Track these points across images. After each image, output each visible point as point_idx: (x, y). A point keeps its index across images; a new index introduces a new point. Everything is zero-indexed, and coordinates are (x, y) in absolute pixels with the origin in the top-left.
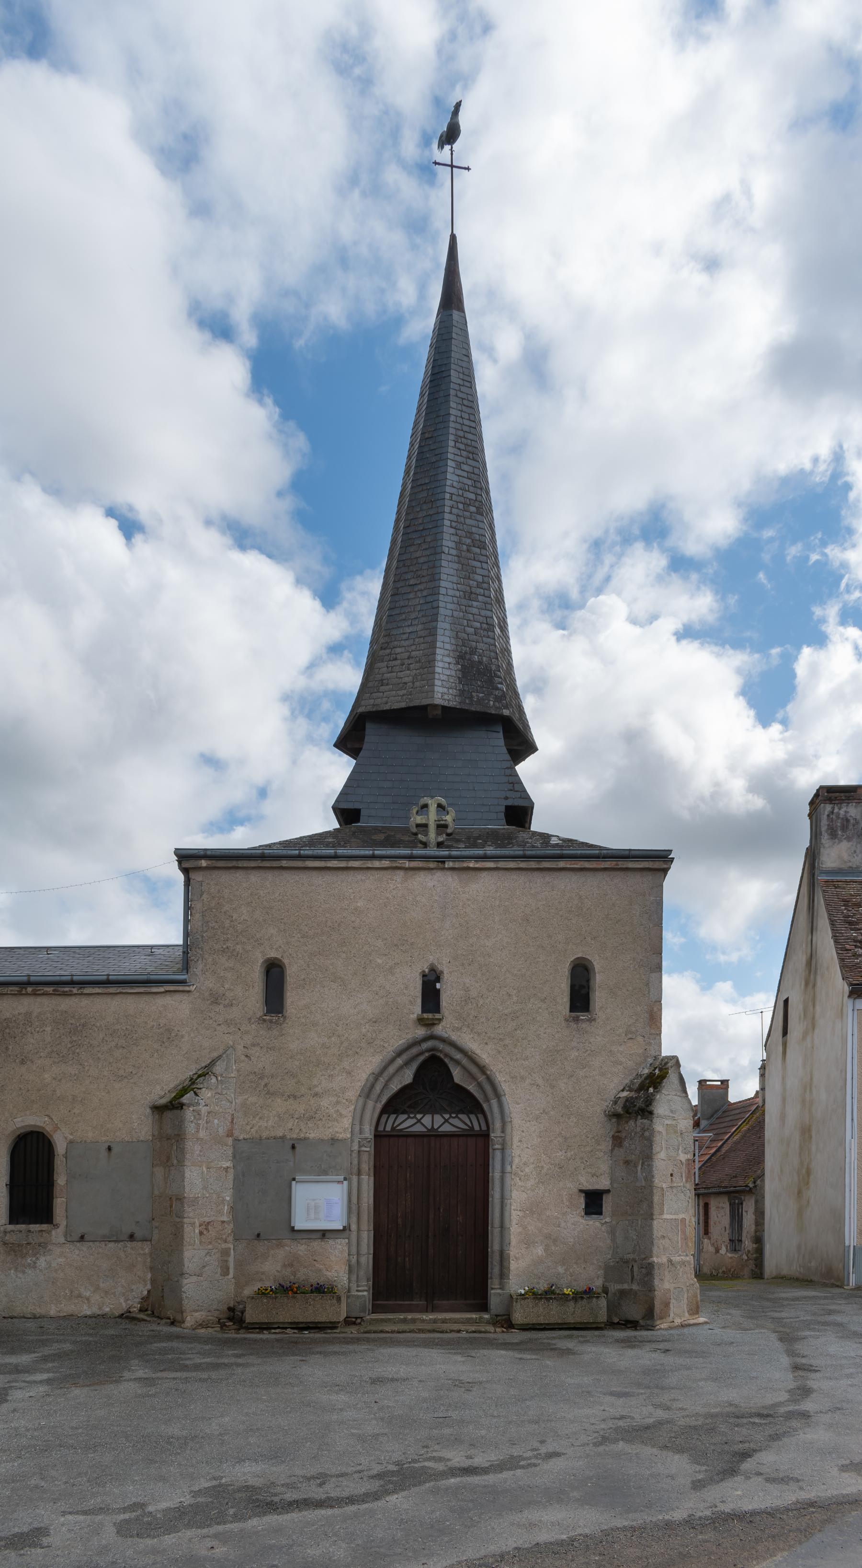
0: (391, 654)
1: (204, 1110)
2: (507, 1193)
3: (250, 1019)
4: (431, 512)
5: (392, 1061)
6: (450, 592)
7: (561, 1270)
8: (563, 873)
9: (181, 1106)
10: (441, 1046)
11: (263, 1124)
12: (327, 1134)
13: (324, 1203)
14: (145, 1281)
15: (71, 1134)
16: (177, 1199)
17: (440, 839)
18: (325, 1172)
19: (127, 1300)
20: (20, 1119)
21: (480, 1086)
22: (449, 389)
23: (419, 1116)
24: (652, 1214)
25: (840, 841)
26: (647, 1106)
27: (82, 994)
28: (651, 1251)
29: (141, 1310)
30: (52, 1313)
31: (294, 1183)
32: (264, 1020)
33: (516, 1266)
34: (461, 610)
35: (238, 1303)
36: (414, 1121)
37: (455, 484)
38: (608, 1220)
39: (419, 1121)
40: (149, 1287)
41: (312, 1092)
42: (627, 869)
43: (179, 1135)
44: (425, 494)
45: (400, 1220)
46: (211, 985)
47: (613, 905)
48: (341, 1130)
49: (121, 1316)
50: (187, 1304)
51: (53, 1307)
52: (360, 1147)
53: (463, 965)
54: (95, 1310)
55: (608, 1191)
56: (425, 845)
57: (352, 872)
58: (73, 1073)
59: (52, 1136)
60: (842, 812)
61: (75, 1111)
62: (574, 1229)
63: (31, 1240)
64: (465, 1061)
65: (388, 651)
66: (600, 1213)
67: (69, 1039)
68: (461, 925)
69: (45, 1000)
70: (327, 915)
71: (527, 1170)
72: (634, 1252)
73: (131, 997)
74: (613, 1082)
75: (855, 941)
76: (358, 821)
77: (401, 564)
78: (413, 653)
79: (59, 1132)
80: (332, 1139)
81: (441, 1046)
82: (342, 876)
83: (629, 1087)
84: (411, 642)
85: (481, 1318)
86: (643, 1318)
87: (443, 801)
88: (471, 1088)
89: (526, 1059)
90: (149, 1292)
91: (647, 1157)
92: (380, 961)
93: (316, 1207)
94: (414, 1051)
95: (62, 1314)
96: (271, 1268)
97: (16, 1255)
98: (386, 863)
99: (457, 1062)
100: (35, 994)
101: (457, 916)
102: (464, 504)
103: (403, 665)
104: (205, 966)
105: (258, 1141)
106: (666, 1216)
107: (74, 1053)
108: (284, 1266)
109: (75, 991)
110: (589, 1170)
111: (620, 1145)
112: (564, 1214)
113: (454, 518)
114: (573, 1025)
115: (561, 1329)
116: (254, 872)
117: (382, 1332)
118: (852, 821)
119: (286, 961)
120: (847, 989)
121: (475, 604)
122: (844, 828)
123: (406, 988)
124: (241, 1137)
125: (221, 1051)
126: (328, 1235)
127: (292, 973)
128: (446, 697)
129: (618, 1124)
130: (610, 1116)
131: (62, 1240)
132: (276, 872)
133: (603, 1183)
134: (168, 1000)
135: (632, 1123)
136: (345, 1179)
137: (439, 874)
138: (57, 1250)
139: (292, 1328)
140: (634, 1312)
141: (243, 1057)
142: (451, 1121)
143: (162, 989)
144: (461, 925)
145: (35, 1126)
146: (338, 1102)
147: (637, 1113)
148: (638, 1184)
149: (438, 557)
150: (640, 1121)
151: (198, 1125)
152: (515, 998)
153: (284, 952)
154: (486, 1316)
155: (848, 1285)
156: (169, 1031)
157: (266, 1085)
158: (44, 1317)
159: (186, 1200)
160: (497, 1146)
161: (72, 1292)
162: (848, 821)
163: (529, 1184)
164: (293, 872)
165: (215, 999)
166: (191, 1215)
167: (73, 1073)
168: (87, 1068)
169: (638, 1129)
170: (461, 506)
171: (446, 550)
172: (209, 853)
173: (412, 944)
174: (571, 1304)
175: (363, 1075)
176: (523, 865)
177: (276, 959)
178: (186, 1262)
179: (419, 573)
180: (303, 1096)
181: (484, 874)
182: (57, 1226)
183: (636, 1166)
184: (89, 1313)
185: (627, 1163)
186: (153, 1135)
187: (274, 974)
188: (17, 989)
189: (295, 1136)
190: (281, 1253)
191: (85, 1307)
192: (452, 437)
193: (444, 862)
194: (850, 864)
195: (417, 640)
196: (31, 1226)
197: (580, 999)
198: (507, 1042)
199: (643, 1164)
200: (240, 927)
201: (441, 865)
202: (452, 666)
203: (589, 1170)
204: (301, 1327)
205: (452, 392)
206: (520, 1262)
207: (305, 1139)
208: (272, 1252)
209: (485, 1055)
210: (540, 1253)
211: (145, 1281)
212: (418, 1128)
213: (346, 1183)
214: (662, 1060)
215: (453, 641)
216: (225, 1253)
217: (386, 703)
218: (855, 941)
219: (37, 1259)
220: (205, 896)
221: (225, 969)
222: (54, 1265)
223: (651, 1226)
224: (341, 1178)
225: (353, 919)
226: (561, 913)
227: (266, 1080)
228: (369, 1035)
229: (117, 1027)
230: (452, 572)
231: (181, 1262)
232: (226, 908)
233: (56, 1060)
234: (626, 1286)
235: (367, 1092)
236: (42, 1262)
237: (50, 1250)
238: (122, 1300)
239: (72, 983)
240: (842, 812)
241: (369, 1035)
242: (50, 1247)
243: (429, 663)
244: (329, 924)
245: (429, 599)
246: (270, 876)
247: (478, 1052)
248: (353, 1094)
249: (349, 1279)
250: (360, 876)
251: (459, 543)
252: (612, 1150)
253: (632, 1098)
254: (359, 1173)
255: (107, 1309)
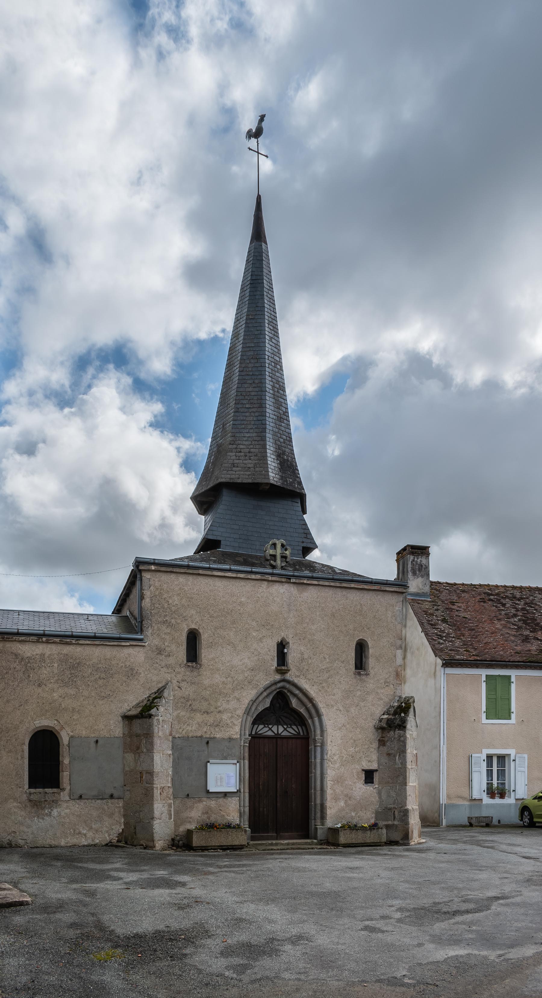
0: (236, 448)
1: (161, 719)
2: (325, 771)
3: (180, 665)
4: (257, 365)
5: (262, 693)
6: (271, 416)
7: (353, 814)
8: (352, 590)
9: (150, 716)
10: (288, 686)
11: (189, 728)
12: (226, 735)
13: (226, 776)
14: (120, 823)
15: (72, 732)
16: (146, 773)
17: (283, 565)
18: (225, 758)
19: (109, 835)
20: (38, 722)
21: (308, 710)
22: (263, 291)
23: (270, 726)
24: (406, 783)
25: (418, 577)
26: (403, 723)
27: (78, 644)
28: (406, 803)
29: (118, 841)
30: (63, 843)
31: (208, 764)
32: (188, 666)
33: (330, 812)
34: (276, 428)
35: (176, 836)
36: (267, 729)
37: (270, 350)
38: (377, 786)
39: (270, 729)
40: (123, 827)
41: (218, 710)
42: (385, 591)
43: (147, 734)
44: (252, 353)
45: (261, 787)
46: (157, 643)
47: (378, 610)
48: (234, 733)
49: (107, 845)
50: (156, 837)
51: (63, 840)
52: (244, 743)
53: (300, 639)
54: (90, 842)
55: (376, 770)
56: (274, 567)
57: (238, 580)
58: (72, 693)
59: (59, 733)
60: (419, 561)
61: (74, 717)
62: (360, 791)
63: (47, 799)
64: (300, 695)
65: (235, 446)
66: (373, 783)
67: (69, 672)
68: (299, 616)
69: (53, 647)
70: (225, 605)
71: (335, 758)
72: (394, 804)
73: (108, 648)
74: (376, 709)
75: (437, 635)
76: (219, 547)
77: (239, 394)
78: (252, 450)
79: (64, 730)
80: (230, 738)
81: (288, 686)
82: (233, 582)
83: (387, 712)
84: (250, 443)
85: (312, 842)
86: (402, 840)
87: (284, 542)
88: (302, 710)
89: (334, 695)
90: (123, 830)
91: (403, 751)
92: (254, 634)
93: (221, 779)
94: (273, 688)
95: (68, 845)
96: (196, 814)
97: (38, 808)
98: (258, 577)
99: (295, 695)
100: (47, 642)
101: (296, 610)
102: (274, 363)
103: (246, 456)
104: (153, 631)
105: (186, 739)
106: (411, 784)
107: (73, 681)
108: (203, 813)
109: (74, 642)
110: (367, 759)
111: (384, 745)
112: (355, 783)
113: (270, 371)
114: (358, 677)
115: (362, 846)
116: (181, 575)
117: (272, 850)
118: (424, 566)
119: (201, 631)
120: (439, 662)
121: (283, 424)
122: (420, 570)
123: (269, 651)
124: (177, 736)
125: (163, 684)
126: (228, 795)
127: (205, 637)
128: (275, 479)
129: (382, 733)
130: (378, 728)
131: (67, 798)
132: (195, 577)
133: (374, 766)
134: (131, 650)
135: (392, 733)
136: (238, 762)
137: (286, 585)
138: (65, 805)
139: (220, 849)
140: (396, 836)
141: (177, 688)
142: (288, 729)
143: (128, 644)
144: (299, 616)
145: (48, 726)
146: (232, 717)
147: (396, 727)
148: (396, 766)
149: (263, 393)
150: (397, 732)
151: (159, 728)
152: (328, 660)
153: (200, 625)
154: (315, 841)
155: (442, 825)
156: (132, 669)
157: (190, 705)
158: (57, 846)
159: (154, 774)
160: (318, 744)
161: (74, 831)
162: (422, 566)
163: (337, 766)
164: (204, 577)
165: (160, 651)
166: (156, 782)
167: (72, 693)
168: (81, 691)
169: (396, 736)
170: (273, 364)
171: (268, 390)
172: (156, 561)
173: (272, 625)
174: (369, 832)
175: (246, 701)
176: (332, 584)
177: (195, 629)
178: (155, 812)
179: (252, 401)
180: (212, 712)
181: (311, 587)
182: (63, 790)
183: (395, 756)
184: (86, 844)
185: (389, 754)
186: (124, 734)
187: (193, 639)
188: (36, 638)
189: (208, 736)
190: (201, 806)
191: (83, 840)
192: (266, 321)
193: (290, 579)
194: (423, 591)
195: (253, 442)
196: (46, 790)
197: (360, 664)
198: (324, 685)
199: (399, 755)
200: (173, 609)
201: (288, 581)
202: (275, 461)
203: (367, 759)
204: (224, 848)
205: (265, 293)
206: (332, 810)
207: (214, 738)
208: (196, 805)
209: (312, 692)
210: (342, 805)
211: (120, 823)
212: (270, 733)
213: (238, 764)
214: (405, 698)
215: (274, 446)
216: (170, 806)
217: (239, 478)
218: (437, 635)
219: (52, 810)
220: (152, 588)
221: (165, 634)
222: (63, 814)
223: (405, 789)
224: (235, 761)
225: (239, 608)
226: (351, 613)
227: (190, 702)
228: (249, 677)
229: (100, 666)
230: (271, 404)
231: (152, 811)
232: (165, 596)
233: (61, 685)
234: (390, 823)
235: (248, 711)
236: (55, 812)
237: (60, 805)
238: (106, 835)
239: (72, 636)
240: (419, 561)
241: (249, 677)
242: (60, 803)
243: (264, 457)
244: (226, 610)
245: (260, 418)
246: (191, 578)
247: (309, 690)
248: (240, 712)
249: (240, 821)
250: (242, 583)
251: (273, 387)
252: (379, 747)
253: (391, 718)
254: (244, 759)
255: (98, 841)
